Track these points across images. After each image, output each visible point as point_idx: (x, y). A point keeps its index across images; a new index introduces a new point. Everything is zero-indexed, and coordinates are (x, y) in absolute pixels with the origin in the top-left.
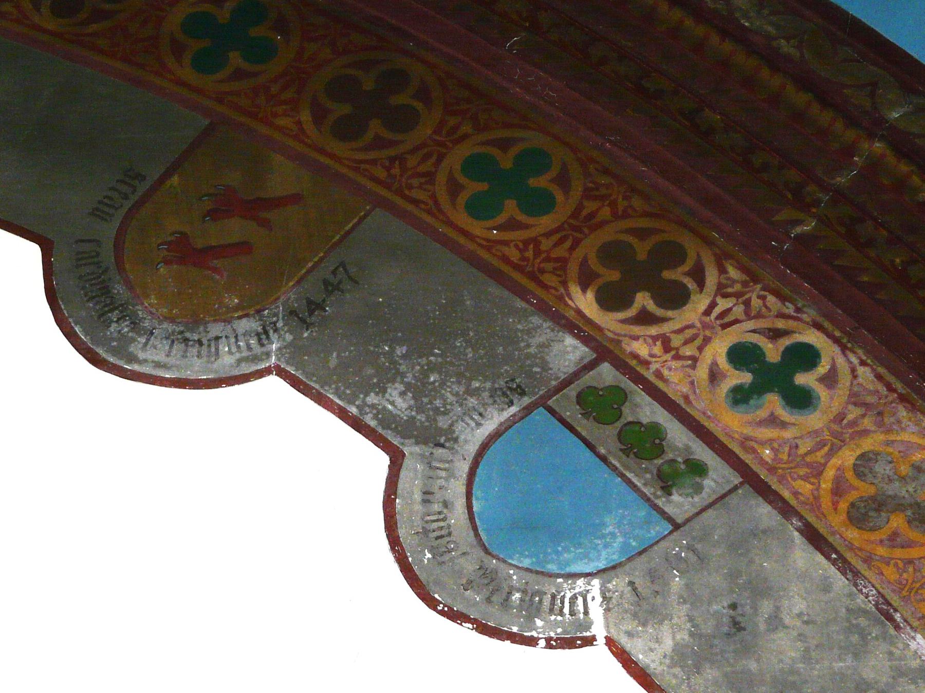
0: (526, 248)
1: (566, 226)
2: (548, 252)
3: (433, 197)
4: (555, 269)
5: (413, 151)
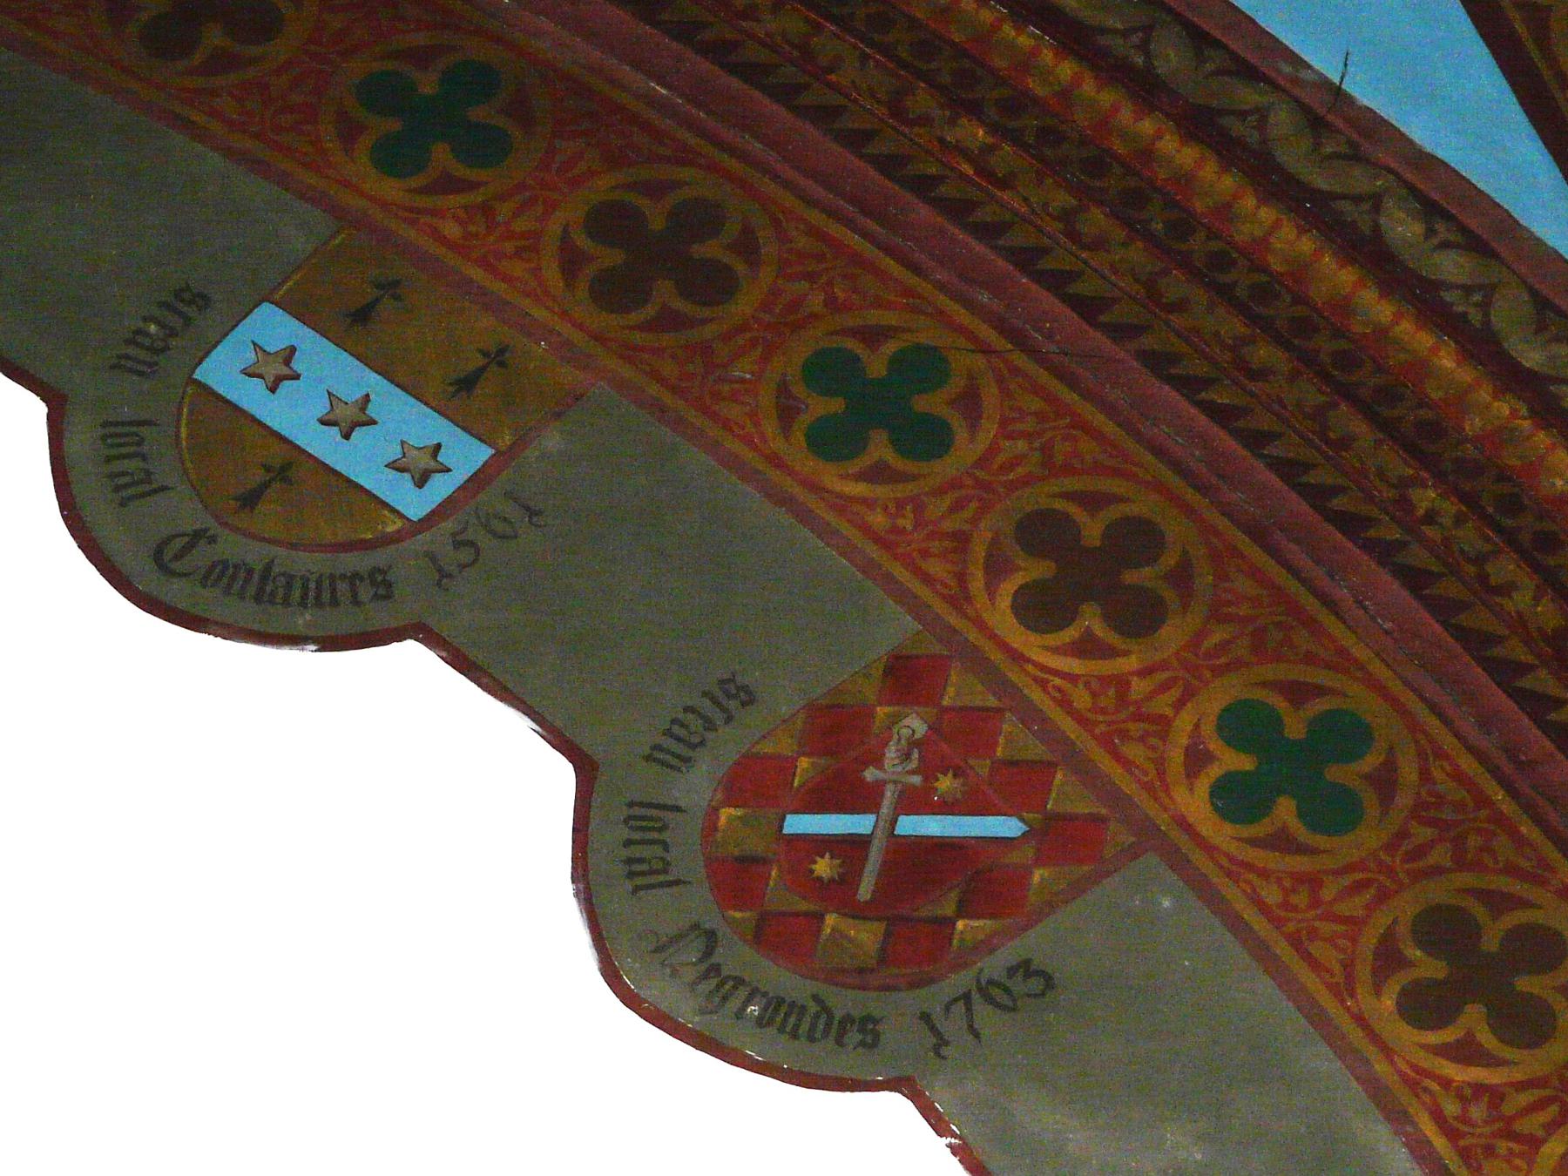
4: (1147, 734)
5: (940, 491)
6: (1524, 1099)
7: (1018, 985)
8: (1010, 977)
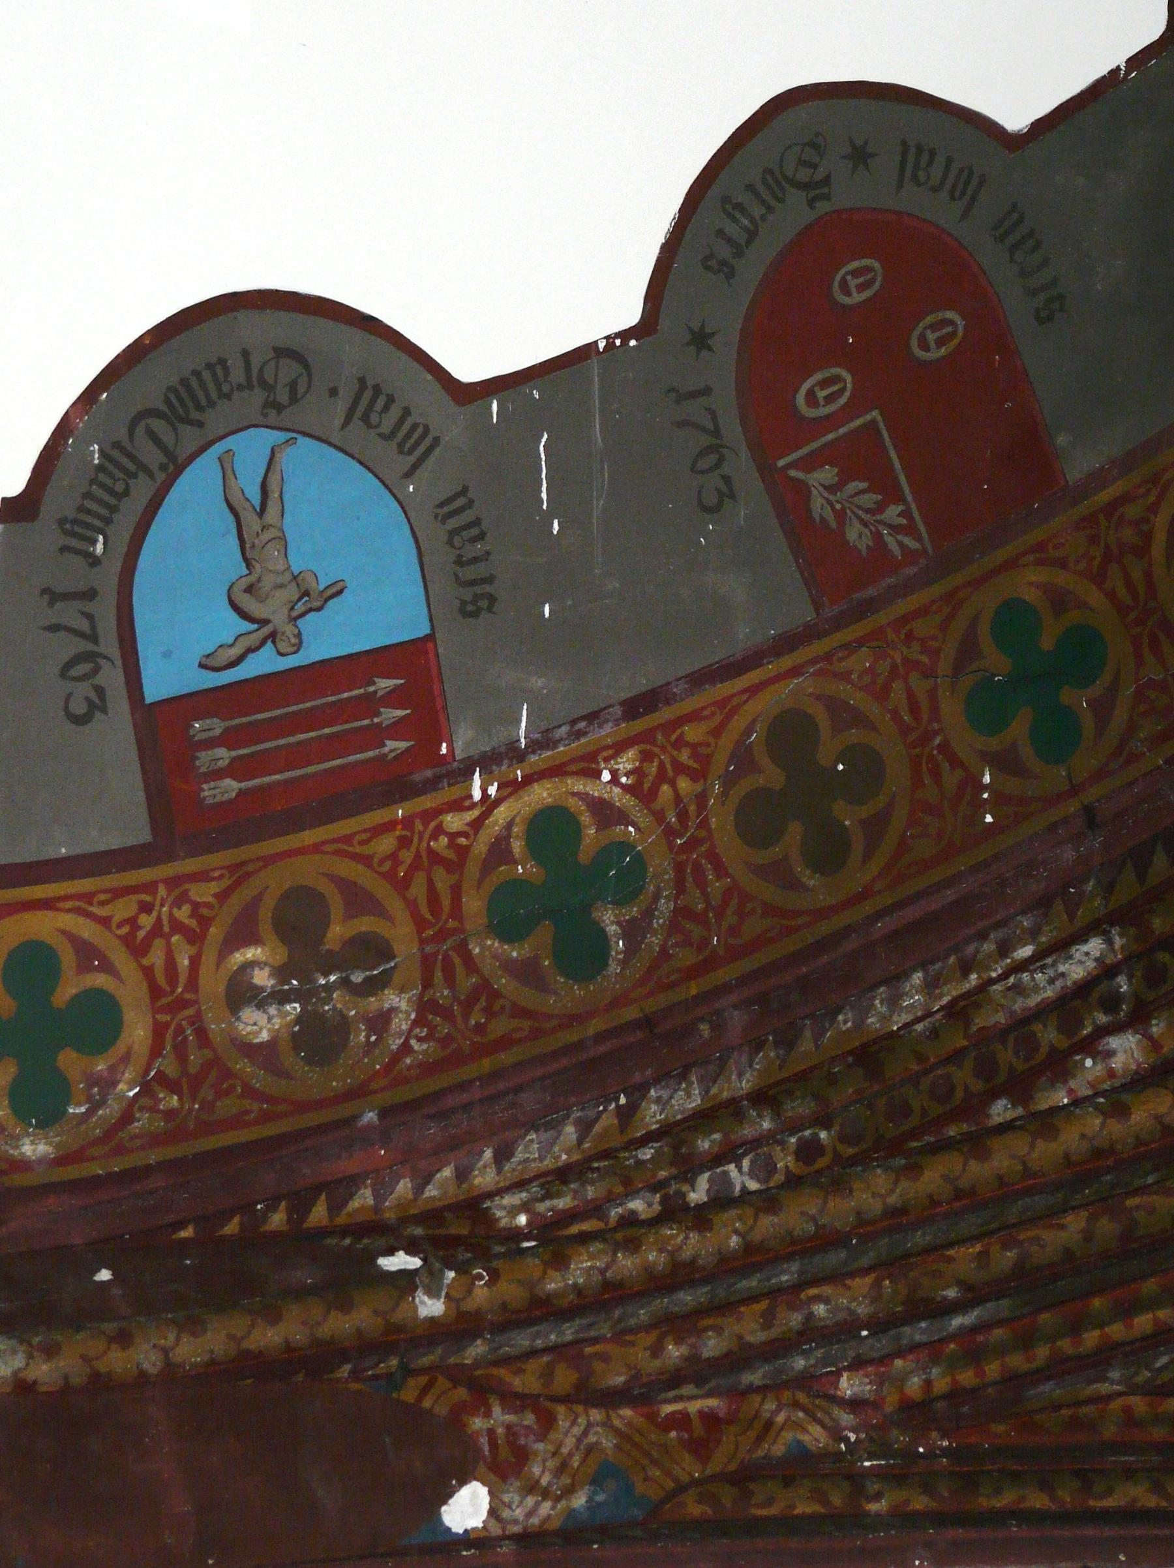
0: (695, 755)
1: (936, 726)
2: (673, 784)
3: (845, 676)
6: (1137, 575)
7: (84, 690)
8: (723, 477)
